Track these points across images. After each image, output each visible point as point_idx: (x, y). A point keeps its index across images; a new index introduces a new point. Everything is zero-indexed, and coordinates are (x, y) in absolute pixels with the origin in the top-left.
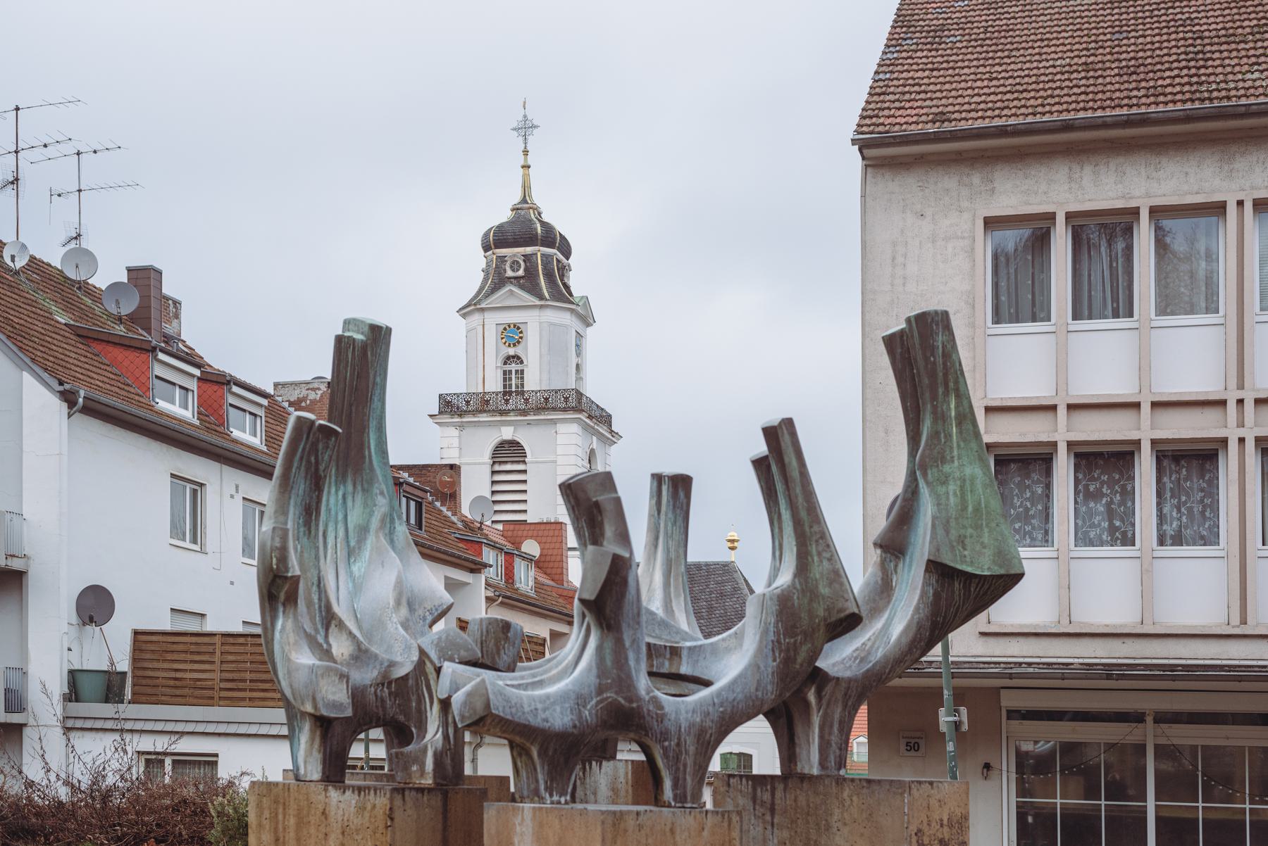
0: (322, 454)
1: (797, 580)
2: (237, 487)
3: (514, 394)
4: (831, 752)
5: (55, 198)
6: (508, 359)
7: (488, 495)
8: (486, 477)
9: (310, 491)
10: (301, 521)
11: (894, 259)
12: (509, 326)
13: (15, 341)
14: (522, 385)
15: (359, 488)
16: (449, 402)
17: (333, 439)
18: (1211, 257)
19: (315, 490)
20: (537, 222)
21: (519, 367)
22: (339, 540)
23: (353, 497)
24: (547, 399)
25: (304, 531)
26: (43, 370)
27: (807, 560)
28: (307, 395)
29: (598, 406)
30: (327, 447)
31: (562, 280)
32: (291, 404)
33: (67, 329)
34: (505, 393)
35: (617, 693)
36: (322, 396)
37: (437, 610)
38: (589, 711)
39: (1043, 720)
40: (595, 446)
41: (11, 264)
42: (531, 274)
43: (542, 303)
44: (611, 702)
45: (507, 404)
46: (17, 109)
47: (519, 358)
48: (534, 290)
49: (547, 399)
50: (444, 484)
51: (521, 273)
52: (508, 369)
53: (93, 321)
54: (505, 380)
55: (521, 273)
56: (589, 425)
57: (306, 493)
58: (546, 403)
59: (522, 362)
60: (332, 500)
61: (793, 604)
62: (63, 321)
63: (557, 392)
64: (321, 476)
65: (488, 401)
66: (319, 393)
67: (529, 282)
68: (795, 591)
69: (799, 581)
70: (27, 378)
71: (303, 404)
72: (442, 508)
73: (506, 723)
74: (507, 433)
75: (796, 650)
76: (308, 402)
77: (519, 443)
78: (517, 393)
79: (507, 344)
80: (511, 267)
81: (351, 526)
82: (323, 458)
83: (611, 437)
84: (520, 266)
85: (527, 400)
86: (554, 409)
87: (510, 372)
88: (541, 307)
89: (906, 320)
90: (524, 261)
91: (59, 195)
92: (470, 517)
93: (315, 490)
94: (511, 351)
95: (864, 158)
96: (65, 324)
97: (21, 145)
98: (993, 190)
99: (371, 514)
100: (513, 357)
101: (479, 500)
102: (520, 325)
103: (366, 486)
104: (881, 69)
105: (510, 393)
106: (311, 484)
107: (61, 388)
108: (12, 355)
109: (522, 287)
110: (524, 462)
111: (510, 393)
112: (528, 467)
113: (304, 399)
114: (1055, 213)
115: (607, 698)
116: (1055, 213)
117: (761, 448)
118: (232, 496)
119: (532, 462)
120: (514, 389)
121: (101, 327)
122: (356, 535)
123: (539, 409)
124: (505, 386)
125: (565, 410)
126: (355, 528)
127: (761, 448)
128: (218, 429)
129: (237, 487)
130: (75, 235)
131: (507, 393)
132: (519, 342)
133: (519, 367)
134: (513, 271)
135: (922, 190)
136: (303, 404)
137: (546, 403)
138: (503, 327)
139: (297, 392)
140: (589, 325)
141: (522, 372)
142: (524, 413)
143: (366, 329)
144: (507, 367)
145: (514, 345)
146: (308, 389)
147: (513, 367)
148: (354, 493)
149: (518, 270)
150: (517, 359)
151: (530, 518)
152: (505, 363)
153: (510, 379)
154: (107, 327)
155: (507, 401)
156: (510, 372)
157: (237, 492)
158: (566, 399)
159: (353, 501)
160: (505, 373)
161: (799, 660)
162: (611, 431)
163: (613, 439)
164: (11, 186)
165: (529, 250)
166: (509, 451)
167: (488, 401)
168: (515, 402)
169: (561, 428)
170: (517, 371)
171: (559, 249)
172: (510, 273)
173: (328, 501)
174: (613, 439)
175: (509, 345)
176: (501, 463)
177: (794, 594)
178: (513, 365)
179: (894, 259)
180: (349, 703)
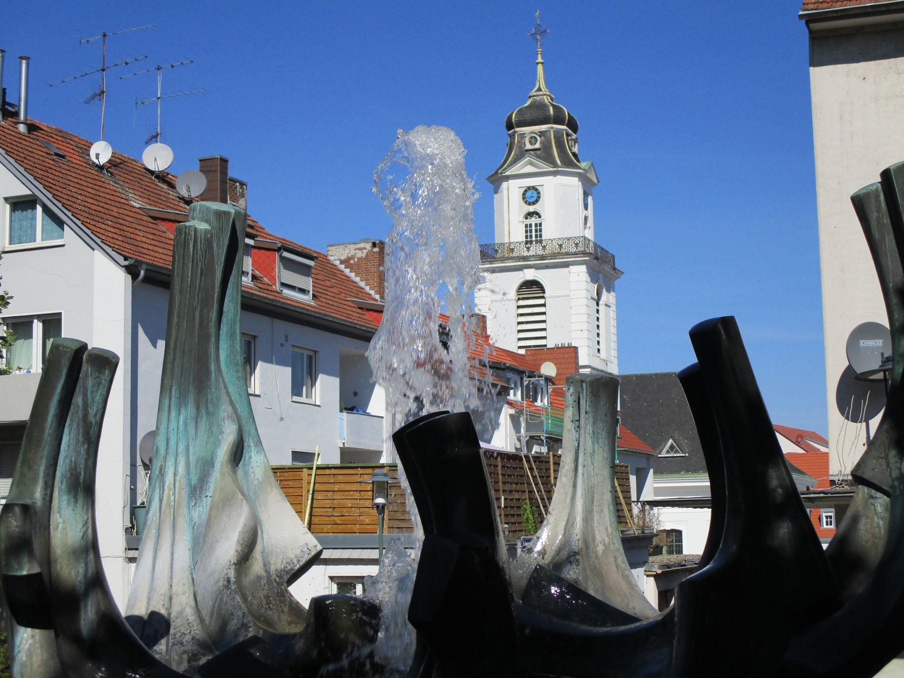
0: (92, 392)
2: (286, 337)
3: (534, 243)
6: (530, 215)
9: (77, 444)
10: (63, 487)
11: (841, 117)
14: (541, 236)
15: (203, 411)
17: (107, 372)
18: (587, 200)
20: (550, 105)
21: (538, 221)
23: (196, 423)
24: (561, 246)
28: (355, 253)
30: (99, 384)
31: (570, 150)
32: (342, 262)
33: (141, 212)
34: (527, 243)
36: (367, 254)
37: (299, 561)
41: (96, 161)
42: (546, 147)
45: (528, 251)
48: (549, 160)
49: (561, 246)
51: (538, 146)
52: (528, 223)
53: (166, 204)
57: (72, 447)
58: (561, 248)
59: (540, 217)
60: (173, 425)
62: (138, 206)
63: (552, 241)
64: (91, 423)
65: (512, 249)
66: (365, 251)
67: (544, 155)
70: (98, 255)
71: (352, 262)
74: (530, 275)
76: (356, 260)
78: (537, 242)
80: (530, 142)
81: (192, 458)
82: (93, 399)
85: (544, 247)
93: (84, 443)
94: (531, 209)
96: (139, 208)
97: (106, 65)
99: (217, 444)
102: (537, 187)
103: (211, 409)
106: (78, 434)
107: (127, 263)
109: (538, 157)
110: (543, 297)
111: (531, 242)
112: (549, 302)
113: (352, 258)
118: (282, 345)
119: (551, 297)
120: (534, 239)
121: (181, 211)
124: (526, 237)
125: (575, 254)
126: (197, 461)
128: (270, 288)
129: (286, 337)
130: (155, 135)
133: (538, 221)
134: (532, 144)
136: (352, 262)
137: (561, 248)
139: (347, 251)
141: (540, 225)
146: (356, 249)
147: (533, 221)
148: (197, 418)
149: (535, 144)
150: (536, 214)
152: (526, 218)
153: (531, 231)
154: (179, 208)
155: (528, 248)
156: (531, 225)
157: (287, 340)
158: (577, 244)
159: (196, 428)
160: (526, 226)
162: (615, 269)
165: (544, 127)
166: (532, 287)
167: (512, 249)
169: (573, 268)
170: (536, 225)
171: (568, 126)
176: (523, 299)
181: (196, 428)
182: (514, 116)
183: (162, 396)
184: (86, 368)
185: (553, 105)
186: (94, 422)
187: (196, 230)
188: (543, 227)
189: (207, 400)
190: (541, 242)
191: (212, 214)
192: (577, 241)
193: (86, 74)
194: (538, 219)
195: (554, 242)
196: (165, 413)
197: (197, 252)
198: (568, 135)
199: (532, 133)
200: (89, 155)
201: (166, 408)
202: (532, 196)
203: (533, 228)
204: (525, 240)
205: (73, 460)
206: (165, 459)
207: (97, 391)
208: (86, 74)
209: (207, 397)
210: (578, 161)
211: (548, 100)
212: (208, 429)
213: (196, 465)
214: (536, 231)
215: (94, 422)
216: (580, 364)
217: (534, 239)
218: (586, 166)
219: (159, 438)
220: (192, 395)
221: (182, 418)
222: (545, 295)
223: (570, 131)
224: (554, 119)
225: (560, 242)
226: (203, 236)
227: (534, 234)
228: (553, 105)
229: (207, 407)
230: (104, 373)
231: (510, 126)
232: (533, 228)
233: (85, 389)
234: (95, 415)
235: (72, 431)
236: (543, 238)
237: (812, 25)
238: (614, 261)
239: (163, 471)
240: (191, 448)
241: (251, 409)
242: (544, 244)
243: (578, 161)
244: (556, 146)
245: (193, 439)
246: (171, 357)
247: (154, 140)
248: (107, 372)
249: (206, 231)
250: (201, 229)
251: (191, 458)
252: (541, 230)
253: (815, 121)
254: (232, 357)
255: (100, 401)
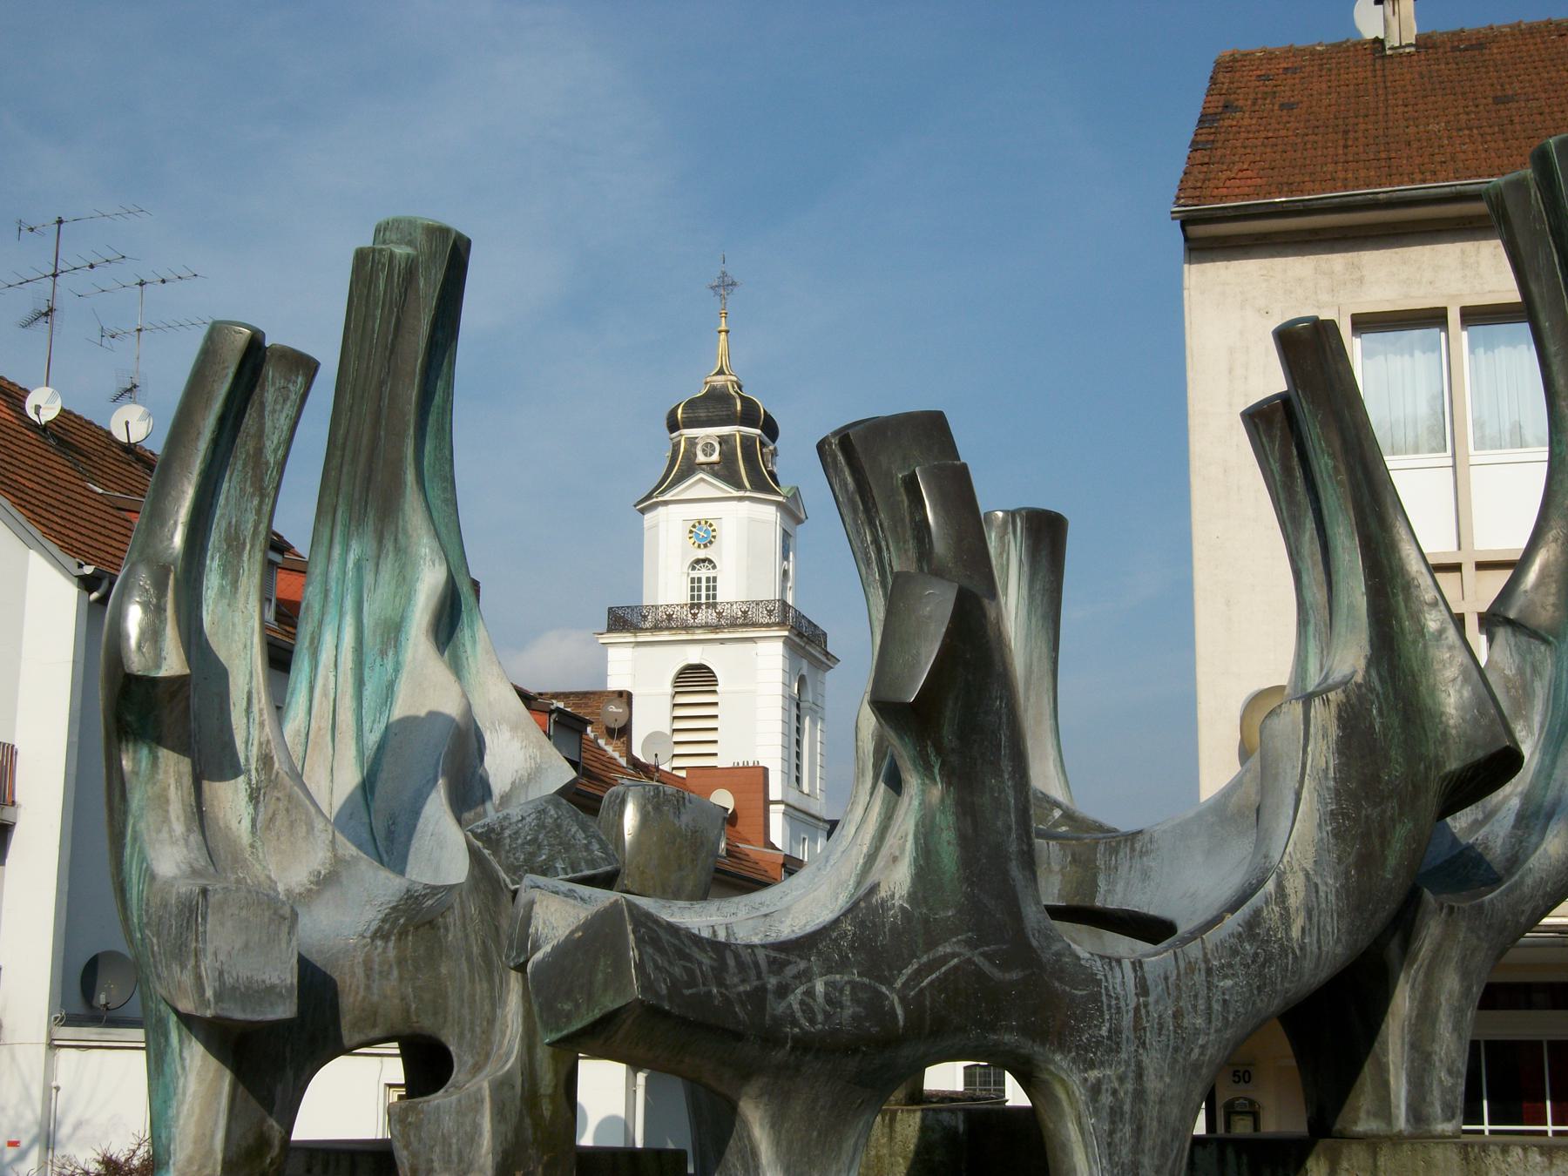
1: (1374, 673)
3: (704, 607)
4: (1435, 1083)
5: (25, 231)
7: (668, 732)
8: (666, 712)
11: (1230, 371)
12: (700, 523)
13: (22, 510)
14: (714, 597)
15: (389, 545)
16: (621, 617)
17: (300, 379)
19: (253, 495)
21: (711, 573)
22: (317, 617)
24: (745, 613)
25: (222, 587)
26: (57, 547)
27: (1391, 627)
29: (809, 622)
35: (969, 943)
38: (898, 992)
39: (1520, 1009)
40: (804, 671)
41: (34, 417)
43: (741, 494)
44: (956, 967)
46: (60, 222)
47: (710, 561)
48: (733, 480)
50: (616, 717)
51: (715, 457)
52: (696, 576)
54: (692, 589)
55: (715, 457)
56: (798, 645)
60: (335, 570)
61: (1372, 726)
67: (725, 471)
68: (1372, 697)
69: (1379, 673)
72: (607, 748)
73: (999, 1090)
74: (694, 655)
75: (1383, 836)
77: (708, 668)
78: (708, 605)
79: (696, 545)
80: (704, 450)
83: (825, 661)
84: (714, 450)
86: (754, 625)
87: (699, 580)
88: (740, 499)
89: (1532, 156)
90: (720, 443)
91: (32, 230)
92: (643, 760)
94: (702, 554)
95: (1186, 239)
97: (61, 266)
98: (1361, 280)
100: (704, 561)
101: (653, 738)
104: (1200, 131)
105: (699, 606)
107: (79, 572)
108: (18, 527)
109: (716, 475)
111: (699, 606)
114: (1445, 309)
115: (945, 959)
116: (1445, 309)
117: (1271, 380)
120: (703, 600)
122: (378, 640)
123: (733, 624)
124: (692, 597)
125: (768, 625)
127: (1271, 380)
131: (695, 606)
132: (711, 542)
134: (706, 455)
135: (1266, 280)
138: (692, 523)
140: (799, 521)
141: (715, 579)
142: (716, 628)
143: (420, 237)
144: (695, 574)
145: (705, 546)
147: (703, 573)
148: (379, 557)
149: (711, 455)
151: (722, 762)
152: (694, 568)
153: (699, 589)
155: (695, 615)
156: (699, 580)
160: (693, 580)
161: (1392, 861)
162: (827, 654)
163: (829, 663)
164: (44, 319)
165: (725, 430)
166: (696, 677)
168: (705, 616)
169: (761, 645)
170: (708, 580)
172: (701, 458)
173: (326, 573)
174: (829, 663)
175: (699, 546)
177: (1372, 703)
178: (704, 570)
179: (1230, 371)
180: (289, 989)
181: (377, 572)
182: (680, 411)
183: (319, 521)
184: (270, 372)
185: (742, 398)
186: (272, 461)
187: (392, 254)
188: (718, 584)
189: (397, 527)
190: (714, 605)
191: (419, 231)
192: (770, 607)
193: (28, 281)
194: (711, 571)
195: (735, 606)
196: (323, 549)
197: (392, 289)
198: (763, 444)
199: (708, 436)
200: (24, 409)
201: (326, 540)
202: (703, 534)
203: (704, 584)
204: (689, 602)
205: (234, 521)
206: (321, 623)
207: (281, 411)
208: (28, 281)
209: (397, 522)
210: (777, 485)
211: (733, 388)
212: (396, 573)
213: (374, 632)
214: (708, 589)
215: (272, 461)
216: (771, 799)
217: (703, 600)
218: (788, 492)
219: (311, 588)
220: (371, 522)
221: (351, 559)
222: (717, 688)
223: (766, 439)
224: (741, 417)
225: (745, 608)
226: (403, 265)
227: (704, 593)
228: (742, 398)
229: (396, 540)
230: (295, 382)
231: (673, 425)
232: (704, 584)
233: (262, 405)
234: (275, 451)
235: (235, 474)
236: (718, 600)
237: (1190, 229)
238: (825, 642)
239: (316, 641)
240: (366, 605)
241: (464, 553)
242: (719, 608)
243: (777, 485)
244: (743, 460)
245: (370, 590)
246: (336, 462)
247: (128, 395)
248: (300, 379)
249: (408, 258)
250: (401, 254)
251: (365, 621)
252: (715, 588)
253: (1190, 375)
254: (437, 467)
255: (285, 428)
